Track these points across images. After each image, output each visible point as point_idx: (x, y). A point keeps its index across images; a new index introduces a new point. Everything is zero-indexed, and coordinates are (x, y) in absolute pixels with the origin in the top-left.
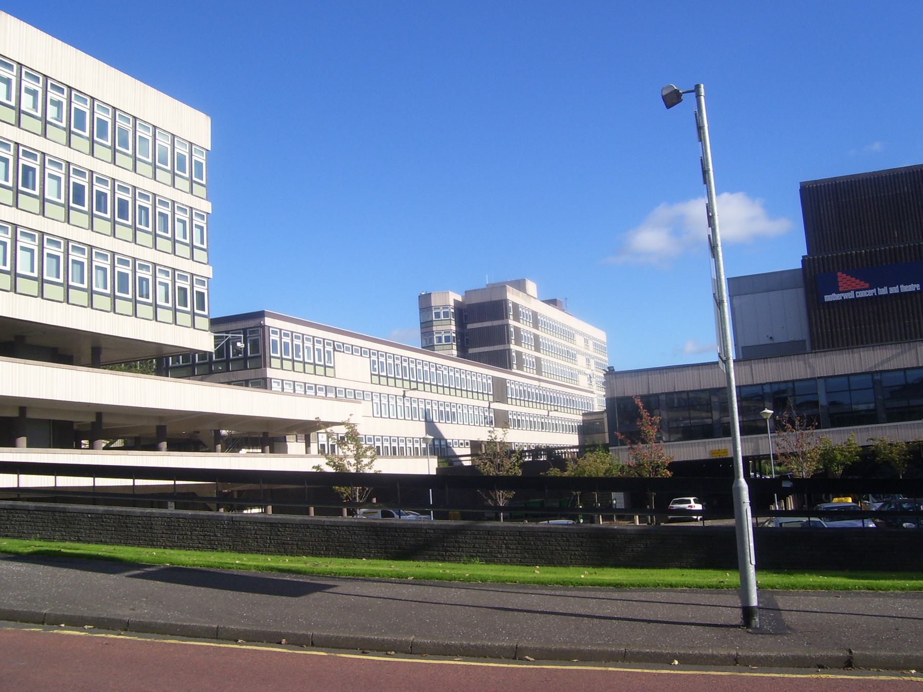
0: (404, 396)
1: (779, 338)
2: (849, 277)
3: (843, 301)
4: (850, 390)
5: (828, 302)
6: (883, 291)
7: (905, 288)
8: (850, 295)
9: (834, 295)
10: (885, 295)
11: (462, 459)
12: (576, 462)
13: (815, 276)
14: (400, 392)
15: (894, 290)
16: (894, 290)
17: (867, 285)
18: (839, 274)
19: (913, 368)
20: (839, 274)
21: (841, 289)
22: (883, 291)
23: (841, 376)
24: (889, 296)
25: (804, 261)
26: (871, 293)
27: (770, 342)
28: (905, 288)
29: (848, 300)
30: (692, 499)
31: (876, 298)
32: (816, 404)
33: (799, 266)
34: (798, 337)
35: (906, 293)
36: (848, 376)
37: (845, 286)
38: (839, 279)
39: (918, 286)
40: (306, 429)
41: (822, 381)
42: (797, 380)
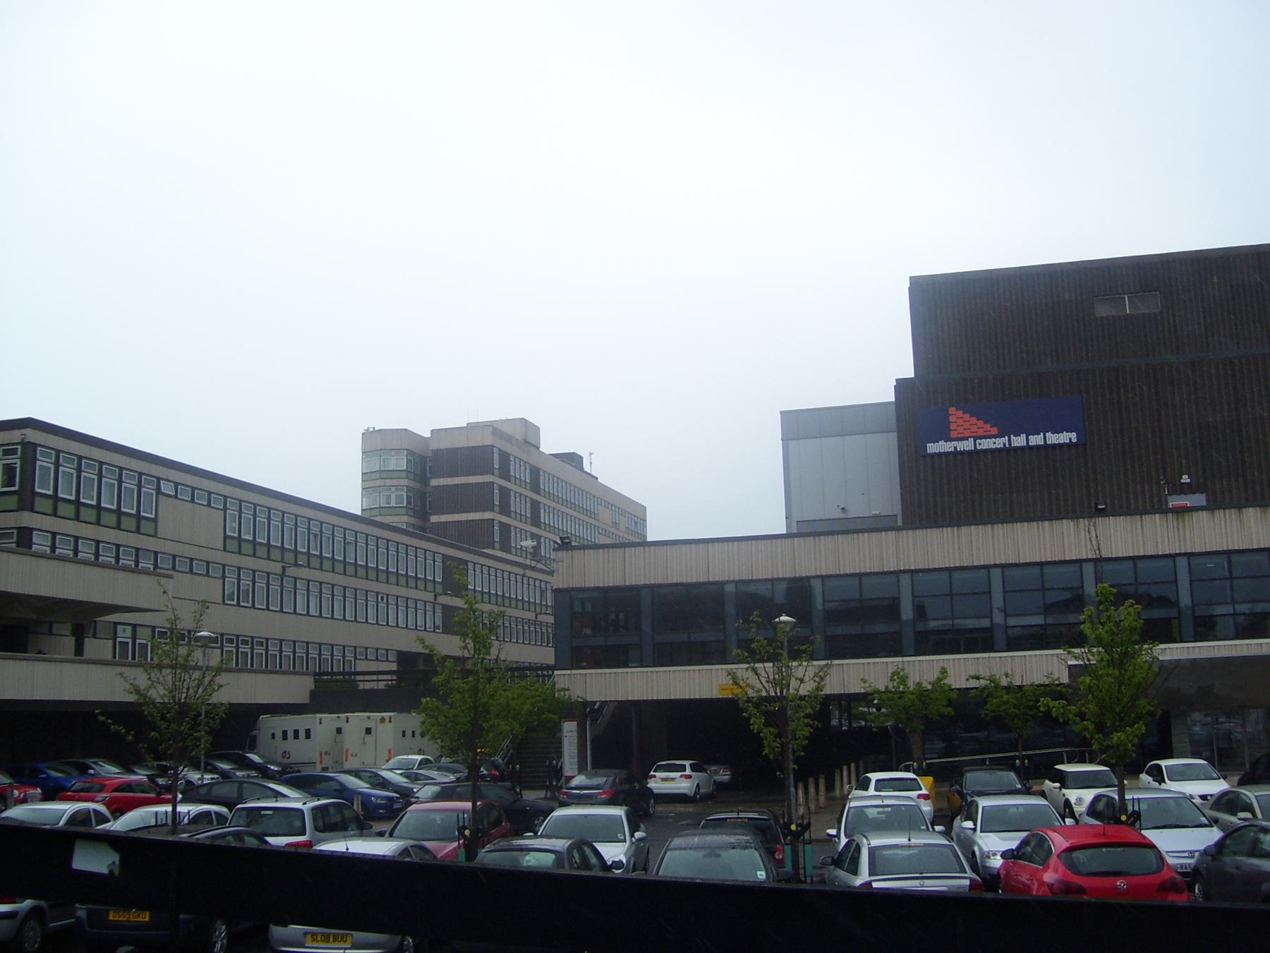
0: (283, 575)
1: (856, 511)
2: (974, 420)
3: (956, 453)
4: (951, 595)
5: (933, 455)
6: (1019, 441)
7: (1053, 438)
8: (967, 445)
9: (942, 443)
10: (1022, 448)
11: (358, 678)
12: (194, 727)
13: (918, 409)
14: (276, 568)
15: (1036, 440)
16: (1036, 440)
17: (994, 431)
18: (952, 410)
19: (1016, 565)
20: (952, 410)
21: (953, 435)
22: (1019, 441)
23: (847, 575)
24: (1029, 448)
25: (901, 385)
26: (1000, 443)
27: (840, 515)
28: (1053, 438)
29: (963, 453)
30: (687, 763)
31: (1008, 451)
32: (1176, 604)
33: (890, 397)
34: (886, 512)
35: (1054, 446)
36: (860, 575)
37: (961, 430)
38: (952, 419)
39: (1073, 436)
40: (83, 619)
41: (908, 576)
42: (867, 574)
